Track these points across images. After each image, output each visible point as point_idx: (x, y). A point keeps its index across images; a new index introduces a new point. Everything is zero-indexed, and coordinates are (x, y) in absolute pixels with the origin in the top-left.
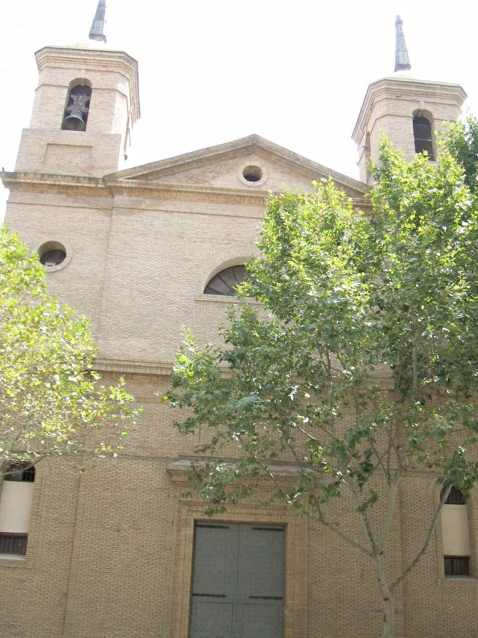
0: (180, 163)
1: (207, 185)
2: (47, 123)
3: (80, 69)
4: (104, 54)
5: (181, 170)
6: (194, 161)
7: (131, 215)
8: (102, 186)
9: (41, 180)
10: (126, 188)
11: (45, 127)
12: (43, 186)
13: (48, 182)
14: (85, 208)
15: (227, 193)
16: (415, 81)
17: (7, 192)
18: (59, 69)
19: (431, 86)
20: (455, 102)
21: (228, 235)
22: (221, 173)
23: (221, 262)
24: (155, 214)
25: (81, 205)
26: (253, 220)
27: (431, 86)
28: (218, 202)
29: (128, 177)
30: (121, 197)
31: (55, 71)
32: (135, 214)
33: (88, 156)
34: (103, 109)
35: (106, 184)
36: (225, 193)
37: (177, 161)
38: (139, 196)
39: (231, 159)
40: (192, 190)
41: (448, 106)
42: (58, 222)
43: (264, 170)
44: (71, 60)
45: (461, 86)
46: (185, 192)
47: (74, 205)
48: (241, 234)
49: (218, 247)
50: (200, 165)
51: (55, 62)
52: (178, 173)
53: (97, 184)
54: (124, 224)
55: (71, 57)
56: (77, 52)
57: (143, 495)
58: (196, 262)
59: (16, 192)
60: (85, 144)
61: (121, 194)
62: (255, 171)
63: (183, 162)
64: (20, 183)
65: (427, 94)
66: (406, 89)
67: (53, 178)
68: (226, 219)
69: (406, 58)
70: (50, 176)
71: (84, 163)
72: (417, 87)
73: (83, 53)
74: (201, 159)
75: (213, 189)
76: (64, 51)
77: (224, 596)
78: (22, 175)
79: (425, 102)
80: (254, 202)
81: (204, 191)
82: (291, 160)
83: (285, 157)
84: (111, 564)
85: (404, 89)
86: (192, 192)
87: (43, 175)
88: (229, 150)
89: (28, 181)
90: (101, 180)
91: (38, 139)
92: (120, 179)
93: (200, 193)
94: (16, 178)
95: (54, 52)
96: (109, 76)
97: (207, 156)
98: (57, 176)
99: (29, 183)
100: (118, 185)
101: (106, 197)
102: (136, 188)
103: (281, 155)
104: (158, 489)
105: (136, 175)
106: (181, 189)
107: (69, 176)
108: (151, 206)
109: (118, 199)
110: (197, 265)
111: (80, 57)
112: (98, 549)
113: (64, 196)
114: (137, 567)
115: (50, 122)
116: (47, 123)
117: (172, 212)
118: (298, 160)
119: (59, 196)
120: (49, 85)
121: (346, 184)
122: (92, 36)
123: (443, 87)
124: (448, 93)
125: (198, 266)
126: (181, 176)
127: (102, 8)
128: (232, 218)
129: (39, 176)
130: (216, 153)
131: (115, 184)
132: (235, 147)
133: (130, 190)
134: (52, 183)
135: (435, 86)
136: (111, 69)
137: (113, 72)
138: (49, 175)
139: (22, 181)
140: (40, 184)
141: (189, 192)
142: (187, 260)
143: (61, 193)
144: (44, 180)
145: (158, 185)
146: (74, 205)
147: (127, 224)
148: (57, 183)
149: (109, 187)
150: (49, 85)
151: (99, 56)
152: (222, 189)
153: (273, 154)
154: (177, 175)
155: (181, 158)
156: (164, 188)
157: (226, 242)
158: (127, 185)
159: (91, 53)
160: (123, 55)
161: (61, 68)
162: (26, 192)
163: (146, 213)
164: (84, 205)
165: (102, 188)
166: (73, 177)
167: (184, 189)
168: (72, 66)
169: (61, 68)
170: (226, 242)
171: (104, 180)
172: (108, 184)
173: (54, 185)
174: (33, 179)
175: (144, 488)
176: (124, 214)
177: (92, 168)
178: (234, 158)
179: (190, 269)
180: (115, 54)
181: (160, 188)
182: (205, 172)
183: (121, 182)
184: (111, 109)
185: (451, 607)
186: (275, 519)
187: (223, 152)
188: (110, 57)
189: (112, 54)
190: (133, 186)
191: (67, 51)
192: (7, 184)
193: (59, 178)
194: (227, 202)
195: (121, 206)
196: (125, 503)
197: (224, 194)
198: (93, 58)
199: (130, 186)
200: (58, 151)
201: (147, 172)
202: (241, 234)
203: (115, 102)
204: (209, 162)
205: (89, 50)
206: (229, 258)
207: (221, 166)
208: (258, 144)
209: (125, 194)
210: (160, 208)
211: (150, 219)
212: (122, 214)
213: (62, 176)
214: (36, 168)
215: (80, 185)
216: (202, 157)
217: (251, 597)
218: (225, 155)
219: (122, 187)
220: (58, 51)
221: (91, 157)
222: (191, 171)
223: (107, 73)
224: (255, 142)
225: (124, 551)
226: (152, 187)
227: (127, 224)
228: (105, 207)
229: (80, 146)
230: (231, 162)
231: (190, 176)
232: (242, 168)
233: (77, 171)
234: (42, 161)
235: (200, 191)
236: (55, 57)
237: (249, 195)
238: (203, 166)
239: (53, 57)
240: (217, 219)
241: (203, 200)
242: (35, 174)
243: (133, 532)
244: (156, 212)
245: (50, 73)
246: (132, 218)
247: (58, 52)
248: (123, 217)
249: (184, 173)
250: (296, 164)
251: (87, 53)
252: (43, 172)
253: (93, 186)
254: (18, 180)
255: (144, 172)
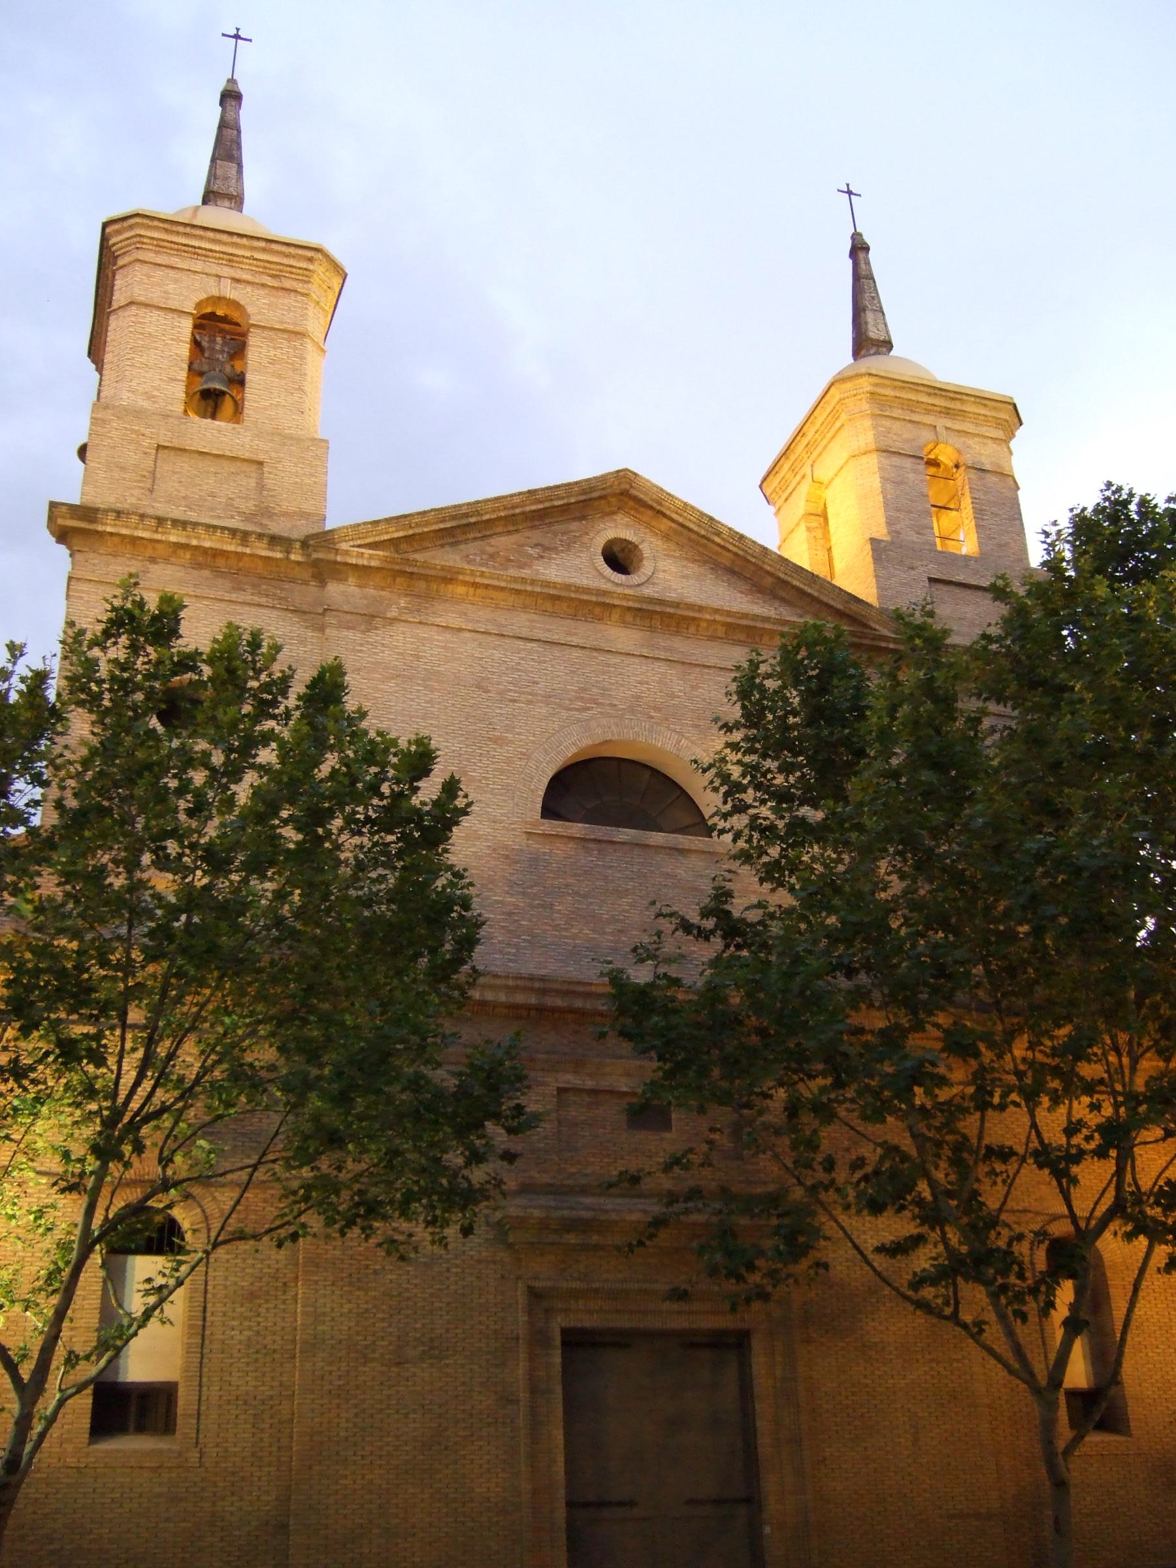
0: (473, 520)
1: (526, 573)
2: (149, 397)
3: (219, 277)
4: (274, 246)
5: (471, 536)
6: (499, 519)
7: (369, 631)
8: (300, 558)
9: (156, 531)
10: (356, 566)
11: (146, 404)
12: (157, 546)
13: (173, 539)
14: (259, 605)
15: (578, 596)
16: (925, 382)
17: (63, 551)
18: (167, 271)
19: (958, 396)
20: (1000, 434)
21: (584, 690)
22: (554, 549)
23: (574, 750)
24: (423, 632)
25: (249, 598)
26: (633, 659)
27: (958, 396)
28: (554, 615)
29: (359, 542)
30: (342, 587)
31: (160, 273)
32: (376, 629)
33: (252, 483)
34: (279, 376)
35: (309, 555)
36: (573, 595)
37: (467, 515)
38: (383, 589)
39: (575, 519)
40: (503, 584)
41: (989, 441)
42: (197, 634)
43: (646, 549)
44: (195, 252)
45: (1016, 401)
46: (487, 586)
47: (234, 597)
48: (610, 690)
49: (564, 714)
50: (511, 528)
51: (157, 252)
52: (466, 541)
53: (288, 552)
54: (354, 650)
55: (196, 243)
56: (210, 234)
57: (448, 1278)
58: (520, 746)
59: (92, 555)
60: (247, 455)
61: (343, 580)
62: (623, 550)
63: (479, 519)
64: (101, 535)
65: (947, 412)
66: (977, 411)
67: (184, 529)
68: (576, 653)
69: (881, 326)
70: (181, 524)
71: (247, 498)
72: (929, 394)
73: (225, 238)
74: (514, 515)
75: (547, 584)
76: (181, 229)
77: (632, 1503)
78: (112, 516)
79: (947, 429)
80: (631, 620)
81: (529, 588)
82: (703, 532)
83: (692, 526)
84: (388, 1444)
85: (905, 396)
86: (502, 589)
87: (161, 521)
88: (573, 500)
89: (124, 531)
90: (298, 545)
91: (133, 431)
92: (344, 546)
93: (518, 592)
94: (93, 520)
95: (156, 228)
96: (286, 301)
97: (528, 509)
98: (196, 525)
99: (124, 537)
100: (339, 558)
101: (305, 583)
102: (378, 569)
103: (681, 520)
104: (479, 1261)
105: (377, 539)
106: (478, 580)
107: (223, 528)
108: (411, 612)
109: (335, 590)
110: (524, 754)
111: (217, 248)
112: (364, 1406)
113: (206, 573)
114: (446, 1449)
115: (156, 393)
116: (149, 397)
117: (460, 630)
118: (719, 534)
119: (195, 573)
120: (147, 305)
121: (816, 594)
122: (210, 197)
123: (983, 399)
124: (988, 413)
125: (526, 756)
126: (471, 548)
127: (230, 133)
128: (587, 652)
129: (153, 523)
130: (547, 504)
131: (331, 557)
132: (585, 493)
133: (363, 571)
134: (183, 540)
135: (964, 397)
136: (288, 284)
137: (296, 291)
138: (176, 522)
139: (109, 529)
140: (151, 541)
141: (495, 588)
142: (498, 741)
143: (199, 566)
144: (163, 533)
145: (425, 565)
146: (234, 597)
147: (360, 651)
148: (194, 542)
149: (316, 563)
150: (147, 305)
151: (264, 250)
152: (567, 587)
153: (664, 515)
154: (462, 547)
155: (475, 507)
156: (441, 574)
157: (579, 704)
158: (360, 562)
159: (244, 241)
160: (138, 220)
161: (172, 268)
162: (115, 556)
163: (401, 627)
164: (257, 599)
165: (298, 563)
166: (233, 532)
167: (486, 582)
168: (198, 266)
169: (172, 268)
170: (579, 704)
171: (305, 544)
172: (315, 556)
173: (185, 547)
174: (136, 528)
175: (448, 1260)
176: (353, 628)
177: (268, 513)
178: (583, 518)
179: (509, 761)
180: (300, 252)
181: (432, 573)
182: (523, 545)
183: (347, 553)
184: (298, 378)
185: (1088, 1499)
186: (724, 1322)
187: (560, 503)
188: (287, 256)
189: (292, 250)
190: (373, 563)
191: (188, 230)
192: (63, 536)
193: (200, 530)
194: (574, 617)
195: (346, 608)
196: (408, 1299)
197: (571, 599)
198: (248, 254)
199: (366, 563)
200: (184, 465)
201: (401, 534)
202: (610, 690)
203: (306, 364)
204: (529, 524)
205: (239, 235)
206: (590, 743)
207: (555, 534)
208: (634, 492)
209: (352, 580)
210: (431, 620)
211: (412, 643)
212: (348, 628)
213: (208, 527)
214: (134, 500)
215: (248, 551)
216: (518, 511)
217: (691, 1502)
218: (565, 509)
219: (346, 564)
220: (166, 226)
221: (261, 487)
222: (493, 541)
223: (280, 293)
224: (628, 487)
225: (414, 1411)
226: (415, 570)
227: (360, 651)
228: (305, 607)
229: (234, 459)
230: (574, 526)
231: (490, 550)
232: (600, 541)
233: (232, 517)
234: (148, 486)
235: (519, 587)
236: (157, 239)
237: (624, 603)
238: (517, 531)
239: (153, 238)
240: (557, 652)
241: (525, 608)
242: (143, 516)
243: (432, 1365)
244: (426, 628)
245: (149, 277)
246: (373, 637)
247: (166, 230)
248: (350, 634)
249: (478, 543)
250: (713, 542)
251: (235, 239)
252: (160, 513)
253: (279, 555)
254: (100, 528)
255: (396, 535)
